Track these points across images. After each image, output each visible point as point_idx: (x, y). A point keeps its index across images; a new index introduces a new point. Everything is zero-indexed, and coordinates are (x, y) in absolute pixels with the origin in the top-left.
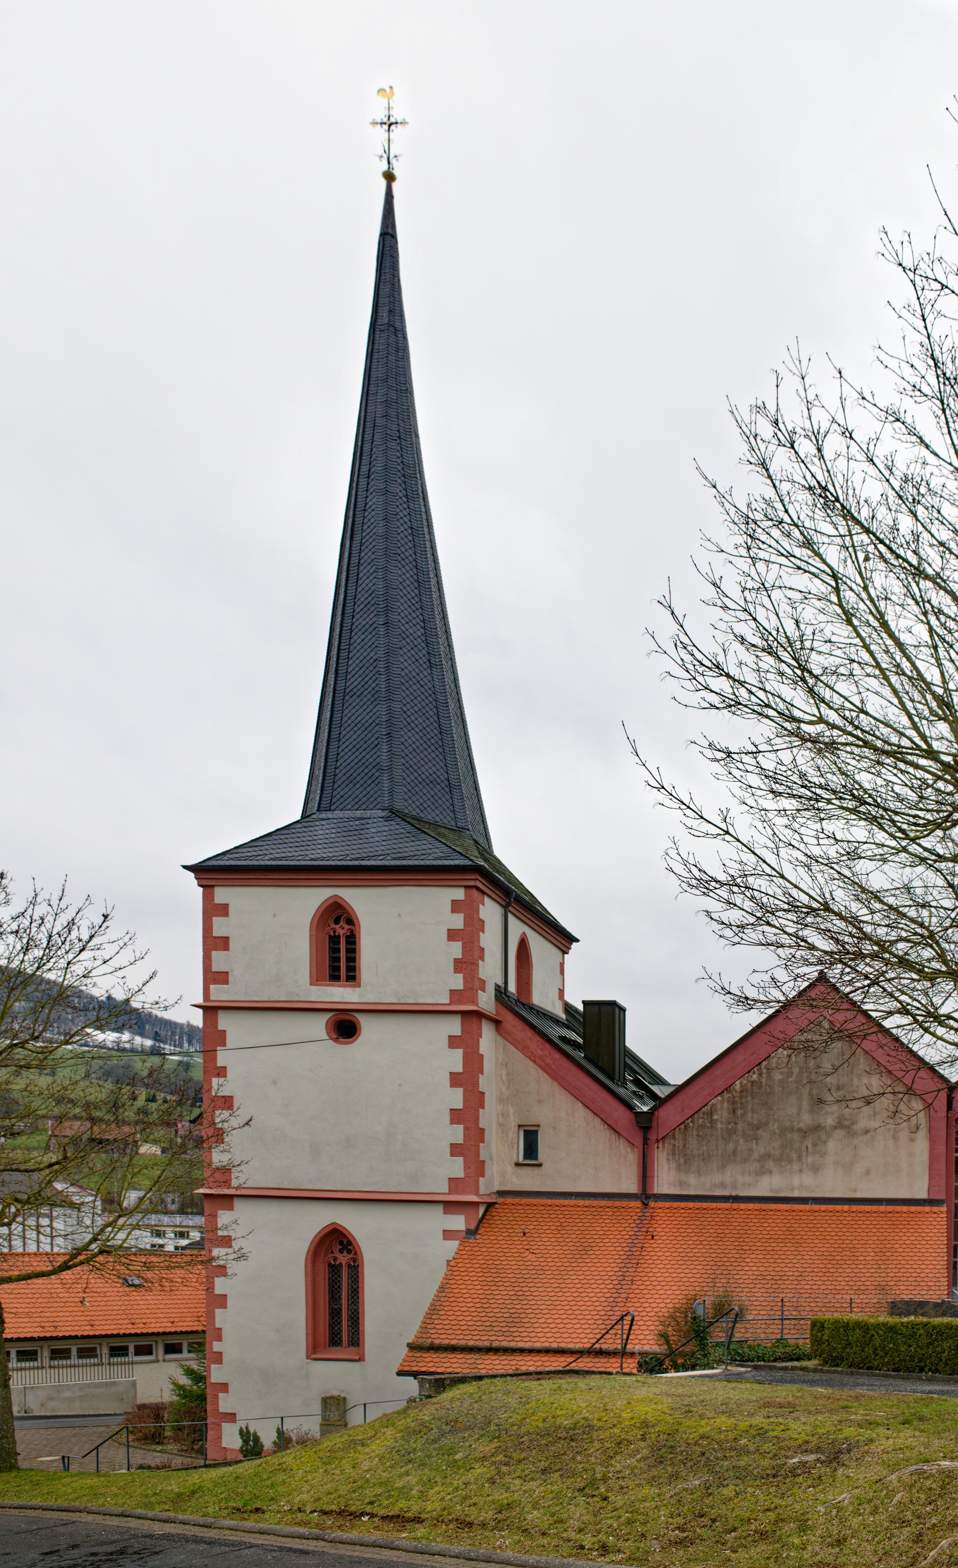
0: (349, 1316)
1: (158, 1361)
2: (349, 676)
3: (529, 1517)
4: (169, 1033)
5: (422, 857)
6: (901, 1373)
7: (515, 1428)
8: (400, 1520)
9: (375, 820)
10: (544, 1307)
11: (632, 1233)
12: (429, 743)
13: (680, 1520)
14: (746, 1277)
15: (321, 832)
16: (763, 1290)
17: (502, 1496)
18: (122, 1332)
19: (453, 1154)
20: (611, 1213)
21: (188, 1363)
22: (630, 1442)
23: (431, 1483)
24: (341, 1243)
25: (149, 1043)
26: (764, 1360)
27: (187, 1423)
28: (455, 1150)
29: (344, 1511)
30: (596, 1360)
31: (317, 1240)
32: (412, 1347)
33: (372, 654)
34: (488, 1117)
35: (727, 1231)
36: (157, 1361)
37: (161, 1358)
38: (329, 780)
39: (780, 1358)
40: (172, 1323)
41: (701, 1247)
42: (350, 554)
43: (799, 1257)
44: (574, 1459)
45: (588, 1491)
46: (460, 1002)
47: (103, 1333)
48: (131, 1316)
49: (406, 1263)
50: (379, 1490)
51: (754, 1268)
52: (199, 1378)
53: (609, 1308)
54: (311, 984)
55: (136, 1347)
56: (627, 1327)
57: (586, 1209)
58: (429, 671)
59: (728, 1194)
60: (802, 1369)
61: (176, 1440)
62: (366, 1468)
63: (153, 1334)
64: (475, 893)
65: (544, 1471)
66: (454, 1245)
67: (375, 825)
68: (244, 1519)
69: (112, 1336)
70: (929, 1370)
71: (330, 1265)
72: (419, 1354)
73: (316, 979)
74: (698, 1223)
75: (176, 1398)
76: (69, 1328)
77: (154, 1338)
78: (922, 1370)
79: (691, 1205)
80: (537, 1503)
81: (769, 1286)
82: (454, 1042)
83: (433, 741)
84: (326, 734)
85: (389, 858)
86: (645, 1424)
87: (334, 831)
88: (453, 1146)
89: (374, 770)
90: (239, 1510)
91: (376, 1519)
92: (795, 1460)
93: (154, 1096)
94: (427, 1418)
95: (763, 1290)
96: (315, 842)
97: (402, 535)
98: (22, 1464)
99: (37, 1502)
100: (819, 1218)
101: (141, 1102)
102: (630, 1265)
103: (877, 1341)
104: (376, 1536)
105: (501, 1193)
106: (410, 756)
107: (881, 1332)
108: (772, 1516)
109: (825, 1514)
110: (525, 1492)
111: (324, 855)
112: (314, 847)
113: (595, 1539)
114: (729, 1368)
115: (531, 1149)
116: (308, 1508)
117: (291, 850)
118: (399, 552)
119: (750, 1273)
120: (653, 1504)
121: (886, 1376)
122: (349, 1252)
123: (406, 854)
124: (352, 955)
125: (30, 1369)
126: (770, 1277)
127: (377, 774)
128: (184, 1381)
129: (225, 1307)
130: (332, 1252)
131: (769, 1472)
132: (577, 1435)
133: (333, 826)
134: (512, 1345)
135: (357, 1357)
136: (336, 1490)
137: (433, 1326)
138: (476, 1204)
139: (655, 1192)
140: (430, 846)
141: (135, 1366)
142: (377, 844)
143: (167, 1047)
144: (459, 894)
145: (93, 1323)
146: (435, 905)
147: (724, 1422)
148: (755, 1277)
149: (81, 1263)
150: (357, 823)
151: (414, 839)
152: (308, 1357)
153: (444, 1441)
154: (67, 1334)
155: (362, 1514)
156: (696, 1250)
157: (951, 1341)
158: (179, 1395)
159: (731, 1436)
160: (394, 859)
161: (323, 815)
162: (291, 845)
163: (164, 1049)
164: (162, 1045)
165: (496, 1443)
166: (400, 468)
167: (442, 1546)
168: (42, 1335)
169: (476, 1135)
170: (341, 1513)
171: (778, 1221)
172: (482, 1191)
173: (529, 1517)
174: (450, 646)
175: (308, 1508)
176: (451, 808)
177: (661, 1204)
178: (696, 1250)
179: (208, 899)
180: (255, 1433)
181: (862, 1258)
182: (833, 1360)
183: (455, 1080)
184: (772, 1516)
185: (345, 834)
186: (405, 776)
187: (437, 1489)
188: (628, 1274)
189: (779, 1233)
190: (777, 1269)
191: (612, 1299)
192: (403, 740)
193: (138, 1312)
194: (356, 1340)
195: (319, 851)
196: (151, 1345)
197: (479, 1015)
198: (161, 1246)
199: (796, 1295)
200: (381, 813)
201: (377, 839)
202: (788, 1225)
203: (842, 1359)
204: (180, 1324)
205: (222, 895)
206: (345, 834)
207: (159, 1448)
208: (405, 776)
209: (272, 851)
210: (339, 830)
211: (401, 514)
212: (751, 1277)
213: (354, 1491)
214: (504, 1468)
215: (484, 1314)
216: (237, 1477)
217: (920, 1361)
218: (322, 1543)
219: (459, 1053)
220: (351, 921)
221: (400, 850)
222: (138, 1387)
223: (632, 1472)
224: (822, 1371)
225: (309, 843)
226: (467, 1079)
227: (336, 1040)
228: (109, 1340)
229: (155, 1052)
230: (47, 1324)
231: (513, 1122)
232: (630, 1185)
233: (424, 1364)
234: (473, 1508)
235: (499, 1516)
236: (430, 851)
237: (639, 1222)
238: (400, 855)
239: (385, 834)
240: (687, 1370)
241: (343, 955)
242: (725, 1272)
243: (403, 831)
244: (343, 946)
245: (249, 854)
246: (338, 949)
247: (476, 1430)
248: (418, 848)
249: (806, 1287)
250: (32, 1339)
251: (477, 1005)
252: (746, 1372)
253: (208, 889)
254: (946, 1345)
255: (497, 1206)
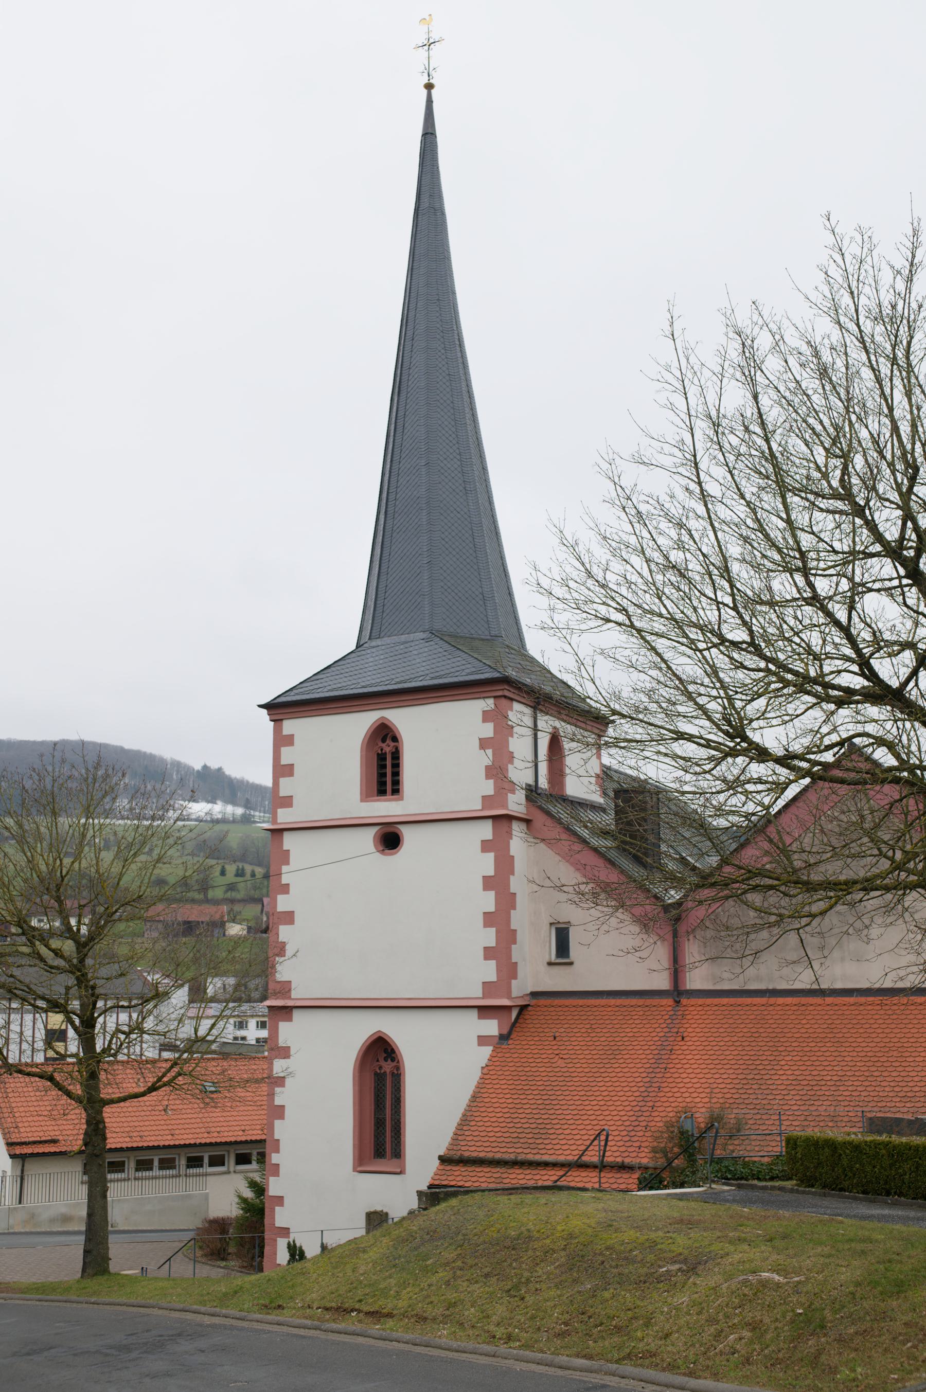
0: (392, 1126)
1: (229, 1172)
2: (396, 515)
3: (466, 1313)
4: (260, 799)
5: (457, 674)
6: (870, 1196)
7: (476, 1237)
8: (376, 1315)
9: (417, 643)
10: (570, 1117)
11: (662, 1034)
12: (465, 563)
13: (567, 1316)
14: (779, 1082)
15: (371, 659)
16: (797, 1097)
17: (452, 1296)
18: (198, 1141)
19: (486, 958)
20: (641, 1013)
21: (251, 1175)
22: (554, 1251)
23: (404, 1285)
24: (386, 1051)
25: (239, 811)
26: (759, 1179)
27: (244, 1238)
28: (489, 953)
29: (340, 1308)
30: (619, 1175)
31: (364, 1049)
32: (443, 1160)
33: (415, 493)
34: (519, 919)
35: (762, 1030)
36: (228, 1172)
37: (232, 1169)
38: (379, 610)
39: (778, 1177)
40: (243, 1131)
41: (732, 1048)
42: (397, 408)
43: (839, 1059)
44: (510, 1265)
45: (512, 1292)
46: (491, 808)
47: (182, 1142)
48: (207, 1125)
49: (444, 1075)
50: (367, 1290)
51: (789, 1072)
52: (259, 1189)
53: (634, 1118)
54: (362, 801)
55: (210, 1157)
56: (603, 1143)
57: (617, 1009)
58: (464, 497)
59: (764, 988)
60: (781, 1189)
61: (239, 1255)
62: (361, 1272)
63: (226, 1143)
64: (504, 702)
65: (487, 1276)
66: (488, 1050)
67: (416, 647)
68: (269, 1314)
69: (190, 1145)
70: (895, 1193)
71: (376, 1074)
72: (449, 1168)
73: (366, 796)
74: (731, 1021)
75: (241, 1212)
76: (153, 1138)
77: (227, 1148)
78: (888, 1194)
79: (725, 1001)
80: (475, 1302)
81: (805, 1092)
82: (486, 846)
83: (468, 560)
84: (377, 569)
85: (428, 678)
86: (571, 1236)
87: (382, 657)
88: (486, 949)
89: (417, 596)
90: (266, 1306)
91: (361, 1315)
92: (664, 1269)
93: (243, 869)
94: (414, 1228)
95: (797, 1097)
96: (366, 670)
97: (441, 383)
98: (113, 1267)
99: (123, 1300)
100: (865, 1012)
101: (230, 877)
102: (658, 1070)
103: (845, 1162)
104: (358, 1327)
105: (534, 994)
106: (448, 578)
107: (848, 1151)
108: (630, 1314)
109: (667, 1313)
110: (469, 1292)
111: (373, 682)
112: (365, 675)
113: (505, 1331)
114: (713, 1186)
115: (563, 947)
116: (315, 1306)
117: (345, 679)
118: (438, 398)
119: (784, 1077)
120: (552, 1304)
121: (855, 1199)
122: (393, 1060)
123: (442, 673)
124: (396, 770)
125: (118, 1180)
126: (805, 1083)
127: (419, 600)
128: (248, 1194)
129: (283, 1119)
130: (378, 1061)
131: (642, 1279)
132: (516, 1245)
133: (381, 652)
134: (537, 1158)
135: (399, 1170)
136: (337, 1290)
137: (463, 1137)
138: (508, 1008)
139: (688, 988)
140: (464, 662)
141: (208, 1178)
142: (418, 665)
143: (257, 814)
144: (489, 704)
145: (173, 1132)
146: (467, 717)
147: (630, 1235)
148: (789, 1082)
149: (164, 1085)
150: (402, 647)
151: (450, 657)
152: (355, 1170)
153: (422, 1249)
154: (151, 1144)
155: (352, 1311)
156: (728, 1053)
157: (910, 1162)
158: (242, 1209)
159: (629, 1247)
160: (432, 678)
161: (374, 643)
162: (346, 675)
163: (254, 816)
164: (252, 812)
165: (459, 1251)
166: (438, 326)
167: (399, 1334)
168: (129, 1145)
169: (507, 937)
170: (338, 1309)
171: (818, 1017)
172: (515, 994)
173: (466, 1313)
174: (484, 469)
175: (315, 1306)
176: (485, 619)
177: (693, 1001)
178: (728, 1053)
179: (277, 731)
180: (301, 1247)
181: (911, 1059)
182: (808, 1181)
183: (488, 883)
184: (630, 1314)
185: (391, 659)
186: (443, 597)
187: (408, 1289)
188: (656, 1080)
189: (818, 1031)
190: (814, 1073)
191: (637, 1108)
192: (442, 565)
193: (214, 1119)
194: (398, 1152)
195: (369, 678)
196: (223, 1156)
197: (509, 818)
198: (244, 1038)
199: (834, 1103)
200: (422, 635)
201: (418, 661)
202: (829, 1022)
203: (816, 1179)
204: (251, 1132)
205: (290, 726)
206: (391, 659)
207: (223, 1264)
208: (443, 597)
209: (330, 683)
210: (386, 656)
211: (440, 365)
212: (785, 1082)
213: (350, 1291)
214: (459, 1273)
215: (512, 1125)
216: (269, 1280)
217: (886, 1183)
218: (318, 1332)
219: (491, 856)
220: (395, 739)
221: (438, 669)
222: (210, 1200)
223: (548, 1277)
224: (797, 1192)
225: (361, 671)
226: (497, 883)
227: (382, 852)
228: (186, 1150)
229: (246, 820)
230: (135, 1134)
231: (546, 920)
232: (662, 982)
233: (453, 1177)
234: (430, 1306)
235: (447, 1313)
236: (463, 667)
237: (669, 1021)
238: (437, 674)
239: (425, 655)
240: (676, 1187)
241: (389, 770)
242: (757, 1077)
243: (441, 650)
244: (389, 762)
245: (311, 688)
246: (384, 768)
247: (448, 1240)
248: (454, 665)
249: (845, 1093)
250: (121, 1150)
251: (507, 808)
252: (728, 1191)
253: (277, 721)
254: (906, 1167)
255: (530, 1008)
